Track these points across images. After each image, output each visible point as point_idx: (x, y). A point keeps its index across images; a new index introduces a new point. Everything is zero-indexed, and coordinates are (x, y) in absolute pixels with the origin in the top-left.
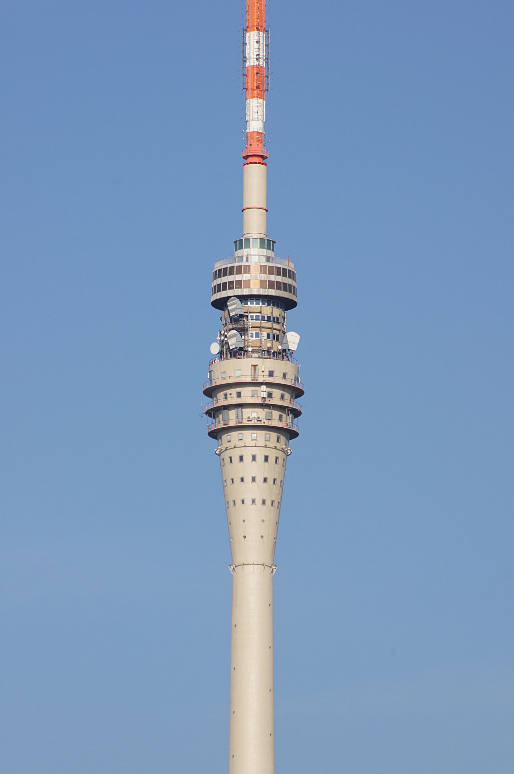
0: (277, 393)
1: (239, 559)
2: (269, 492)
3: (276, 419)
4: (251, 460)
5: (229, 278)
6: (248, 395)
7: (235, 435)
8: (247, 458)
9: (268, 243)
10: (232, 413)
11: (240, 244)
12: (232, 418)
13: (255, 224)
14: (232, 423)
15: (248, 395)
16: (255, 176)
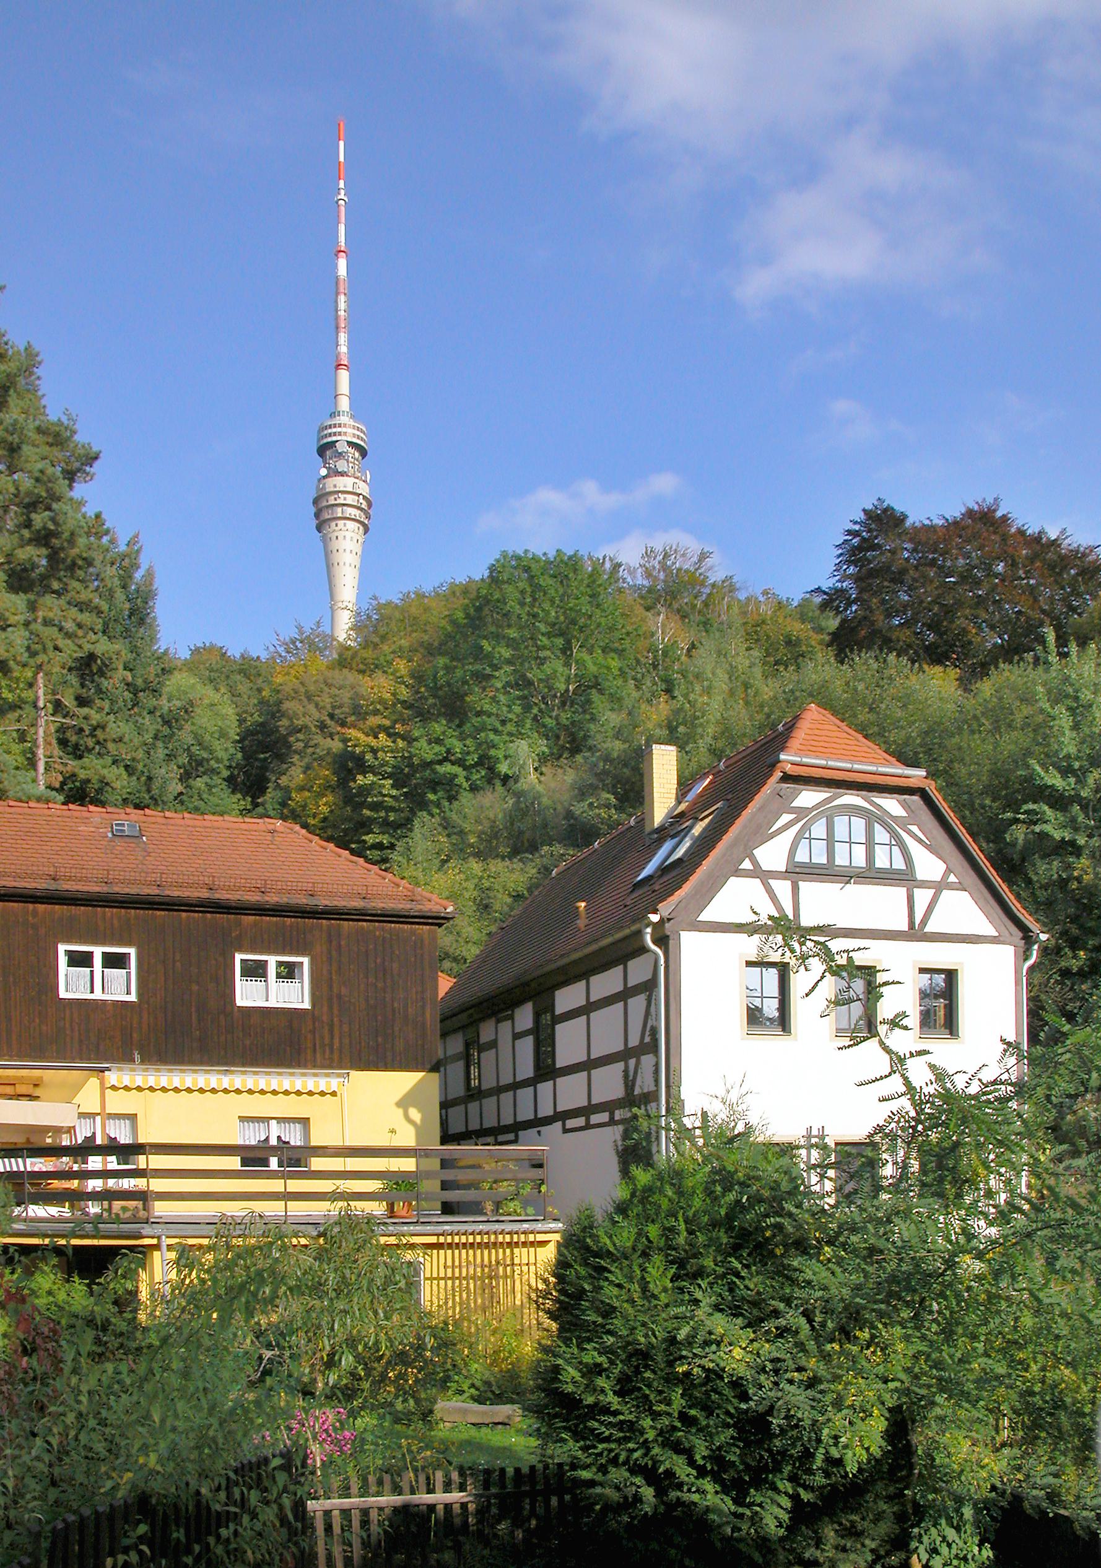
5: (334, 430)
6: (350, 499)
7: (341, 523)
8: (348, 538)
9: (352, 417)
10: (339, 509)
11: (333, 415)
12: (339, 512)
13: (344, 404)
14: (340, 515)
15: (350, 499)
16: (344, 376)
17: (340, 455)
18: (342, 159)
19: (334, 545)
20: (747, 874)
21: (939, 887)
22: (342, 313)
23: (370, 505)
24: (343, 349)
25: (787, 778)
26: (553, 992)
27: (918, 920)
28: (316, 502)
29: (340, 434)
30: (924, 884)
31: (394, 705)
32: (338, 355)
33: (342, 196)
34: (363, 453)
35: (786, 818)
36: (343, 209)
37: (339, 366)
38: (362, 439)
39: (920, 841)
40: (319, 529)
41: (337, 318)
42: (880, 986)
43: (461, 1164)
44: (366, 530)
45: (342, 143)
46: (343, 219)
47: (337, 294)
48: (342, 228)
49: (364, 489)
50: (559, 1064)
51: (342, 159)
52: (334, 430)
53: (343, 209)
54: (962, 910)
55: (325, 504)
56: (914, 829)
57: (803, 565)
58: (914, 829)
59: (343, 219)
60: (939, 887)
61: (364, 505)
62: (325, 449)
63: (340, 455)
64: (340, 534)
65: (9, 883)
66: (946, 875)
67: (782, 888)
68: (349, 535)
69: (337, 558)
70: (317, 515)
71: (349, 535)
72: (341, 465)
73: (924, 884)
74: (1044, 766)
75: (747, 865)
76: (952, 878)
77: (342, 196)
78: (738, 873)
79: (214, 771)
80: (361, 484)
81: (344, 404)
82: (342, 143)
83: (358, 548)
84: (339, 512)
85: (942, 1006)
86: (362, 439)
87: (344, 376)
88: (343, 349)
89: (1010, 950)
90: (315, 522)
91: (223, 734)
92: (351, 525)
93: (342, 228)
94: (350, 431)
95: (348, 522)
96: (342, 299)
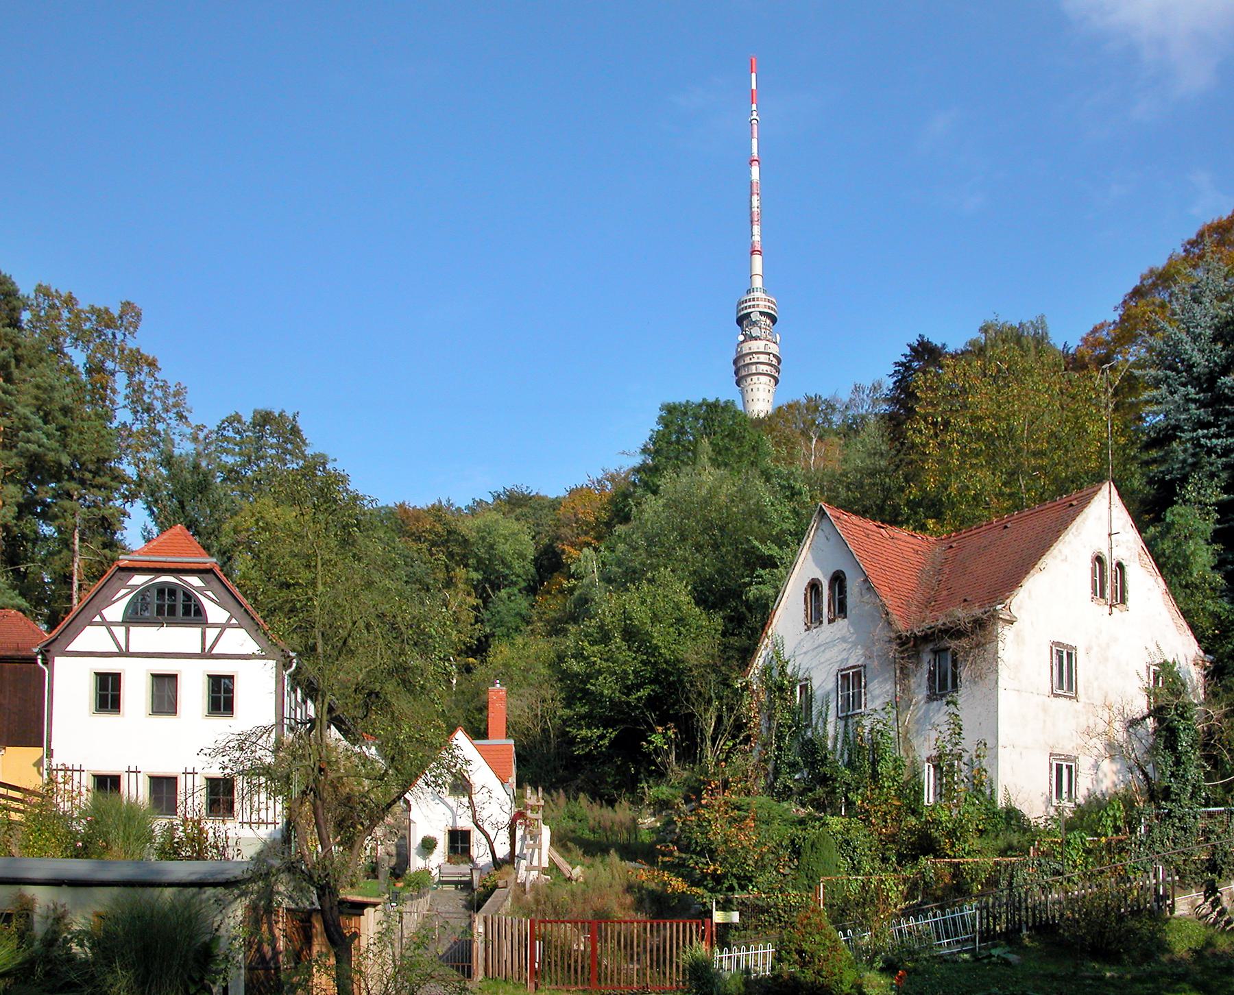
6: (763, 358)
7: (755, 378)
9: (765, 292)
11: (749, 292)
12: (753, 369)
13: (758, 282)
15: (763, 358)
16: (757, 260)
17: (754, 323)
18: (754, 87)
19: (750, 396)
20: (98, 624)
21: (223, 627)
22: (755, 210)
23: (779, 361)
24: (757, 238)
25: (121, 569)
27: (207, 647)
28: (735, 362)
30: (214, 625)
31: (597, 526)
32: (752, 244)
33: (755, 116)
34: (774, 320)
35: (123, 592)
36: (755, 127)
37: (752, 253)
39: (212, 600)
40: (738, 383)
41: (751, 214)
45: (754, 75)
46: (755, 135)
47: (752, 194)
48: (755, 142)
49: (774, 349)
51: (754, 87)
53: (755, 127)
54: (239, 640)
56: (209, 593)
58: (209, 593)
59: (755, 135)
60: (223, 627)
61: (775, 362)
62: (743, 320)
63: (754, 323)
65: (3, 653)
66: (230, 619)
67: (120, 632)
68: (761, 387)
70: (736, 373)
71: (761, 387)
72: (755, 331)
73: (214, 625)
74: (763, 542)
75: (98, 619)
76: (234, 621)
77: (755, 116)
78: (92, 624)
79: (515, 584)
80: (771, 345)
81: (758, 282)
82: (754, 75)
85: (221, 697)
88: (757, 238)
89: (272, 663)
90: (734, 379)
91: (522, 556)
92: (764, 379)
93: (755, 142)
94: (761, 303)
95: (762, 377)
96: (755, 198)
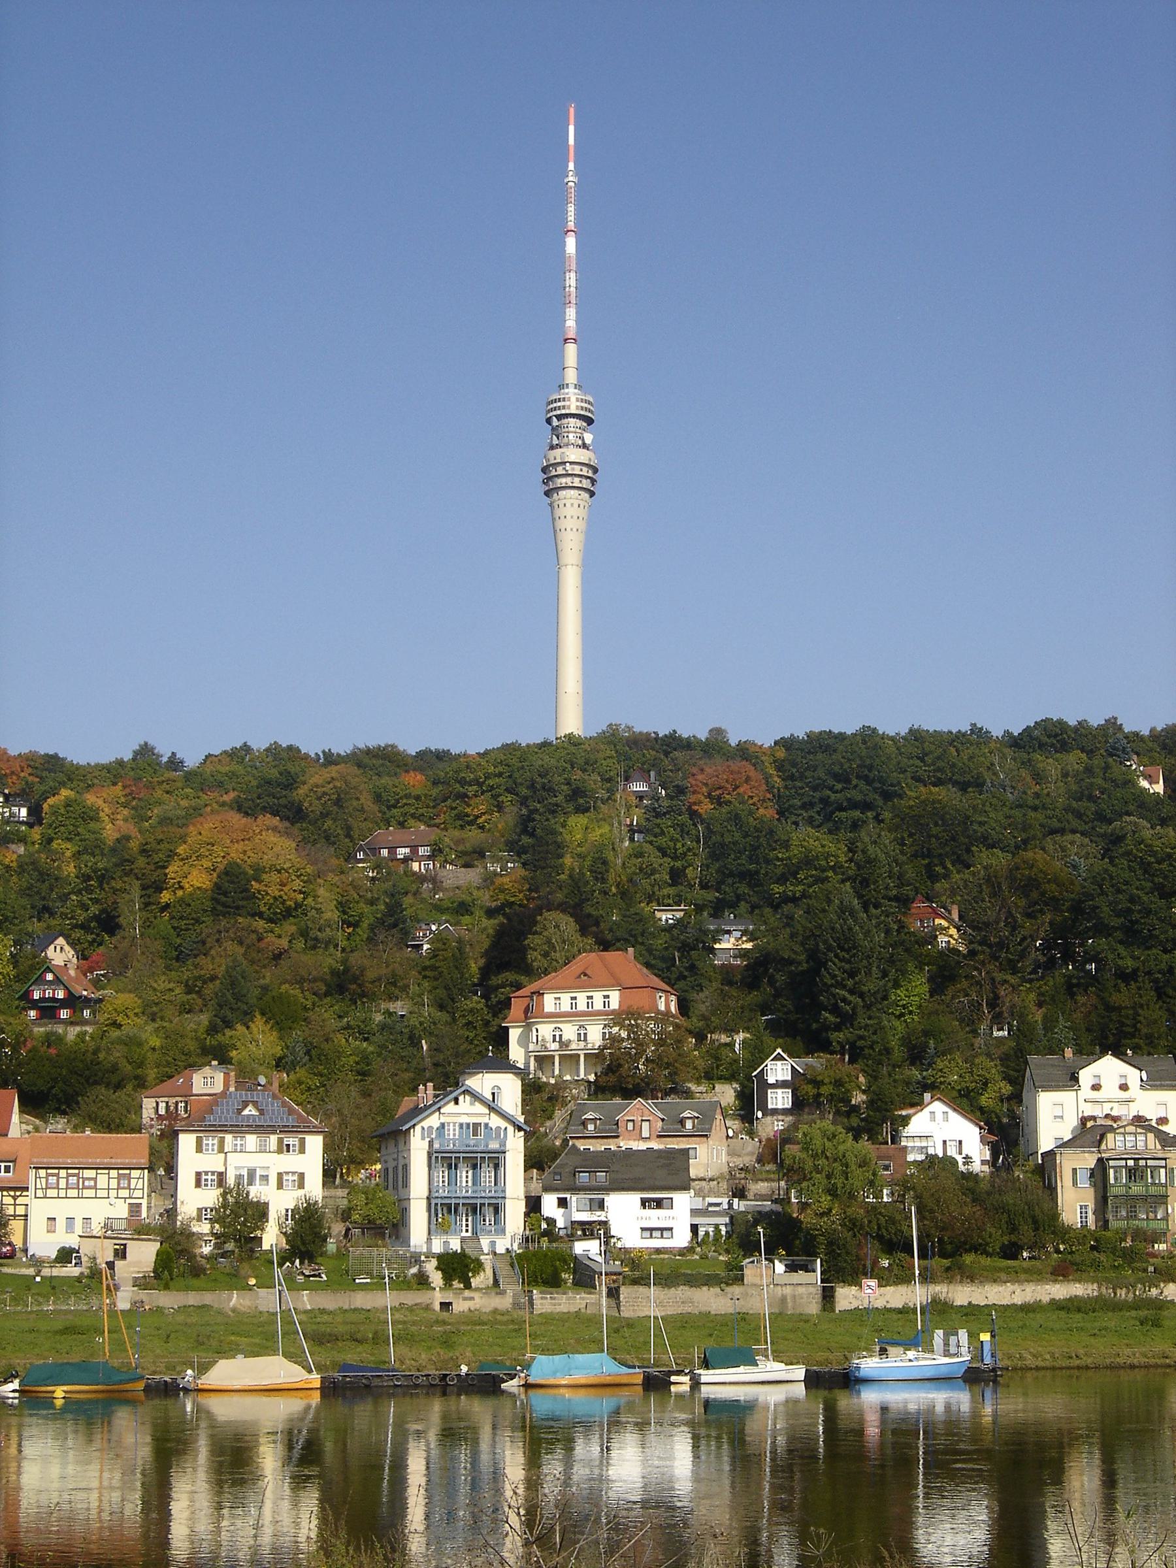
0: (585, 469)
1: (562, 562)
2: (581, 524)
3: (586, 484)
4: (572, 507)
5: (559, 404)
7: (562, 493)
13: (571, 376)
16: (571, 350)
19: (559, 512)
26: (1103, 1053)
29: (564, 407)
34: (590, 421)
38: (590, 411)
42: (467, 1092)
43: (1124, 1472)
44: (592, 494)
50: (194, 1092)
52: (559, 404)
55: (553, 473)
57: (562, 1210)
64: (561, 503)
69: (561, 524)
77: (571, 179)
81: (571, 376)
83: (583, 513)
84: (563, 481)
86: (590, 411)
87: (571, 350)
